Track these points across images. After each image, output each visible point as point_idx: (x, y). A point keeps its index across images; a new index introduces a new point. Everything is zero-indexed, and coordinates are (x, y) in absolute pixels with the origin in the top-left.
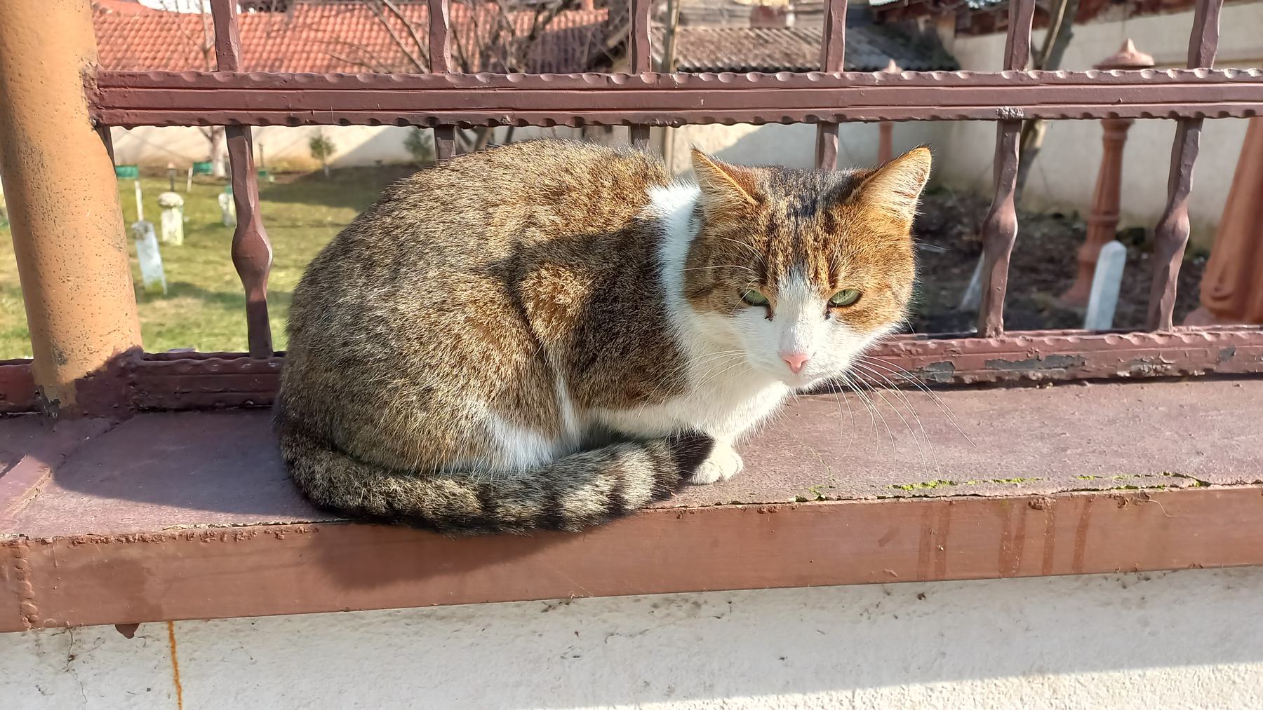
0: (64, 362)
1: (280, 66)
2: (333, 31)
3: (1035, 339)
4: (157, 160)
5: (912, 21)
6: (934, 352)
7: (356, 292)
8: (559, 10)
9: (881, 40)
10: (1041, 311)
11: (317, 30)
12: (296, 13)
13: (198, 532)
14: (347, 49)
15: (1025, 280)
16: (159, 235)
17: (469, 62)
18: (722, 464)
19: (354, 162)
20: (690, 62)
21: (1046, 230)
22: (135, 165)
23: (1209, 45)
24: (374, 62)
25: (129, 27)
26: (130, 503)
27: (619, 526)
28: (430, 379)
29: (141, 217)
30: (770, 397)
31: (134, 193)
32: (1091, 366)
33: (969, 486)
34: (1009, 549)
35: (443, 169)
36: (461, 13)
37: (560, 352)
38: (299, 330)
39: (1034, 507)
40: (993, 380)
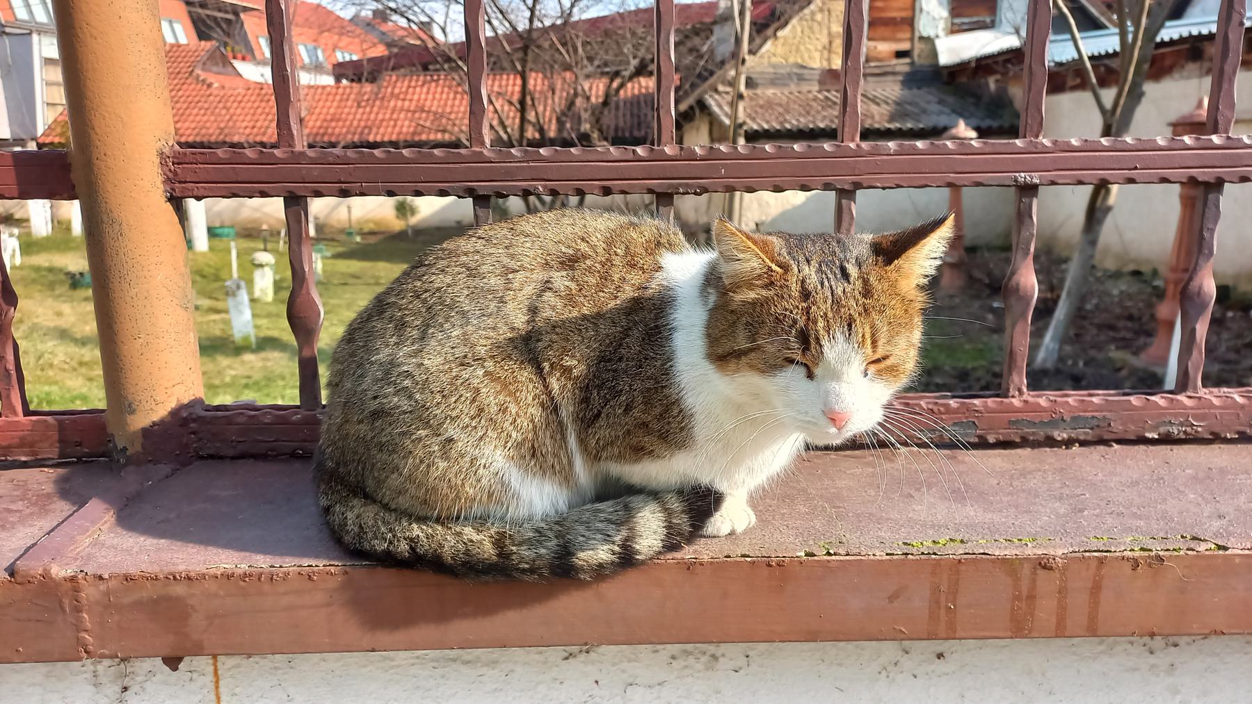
0: (133, 412)
1: (369, 134)
2: (419, 100)
3: (1059, 399)
4: (255, 221)
5: (983, 80)
6: (956, 411)
7: (387, 351)
8: (631, 78)
9: (950, 100)
10: (1119, 370)
11: (404, 100)
12: (385, 84)
13: (240, 571)
14: (432, 118)
15: (1103, 338)
16: (250, 291)
17: (546, 127)
18: (733, 516)
19: (435, 222)
20: (759, 124)
21: (1123, 288)
22: (232, 227)
23: (1227, 113)
24: (456, 129)
25: (232, 99)
26: (179, 543)
27: (632, 576)
28: (451, 431)
29: (235, 275)
30: (779, 454)
31: (229, 252)
32: (1117, 427)
33: (980, 544)
34: (1020, 608)
35: (471, 236)
36: (539, 81)
37: (571, 409)
38: (337, 385)
39: (1045, 567)
40: (1018, 440)
